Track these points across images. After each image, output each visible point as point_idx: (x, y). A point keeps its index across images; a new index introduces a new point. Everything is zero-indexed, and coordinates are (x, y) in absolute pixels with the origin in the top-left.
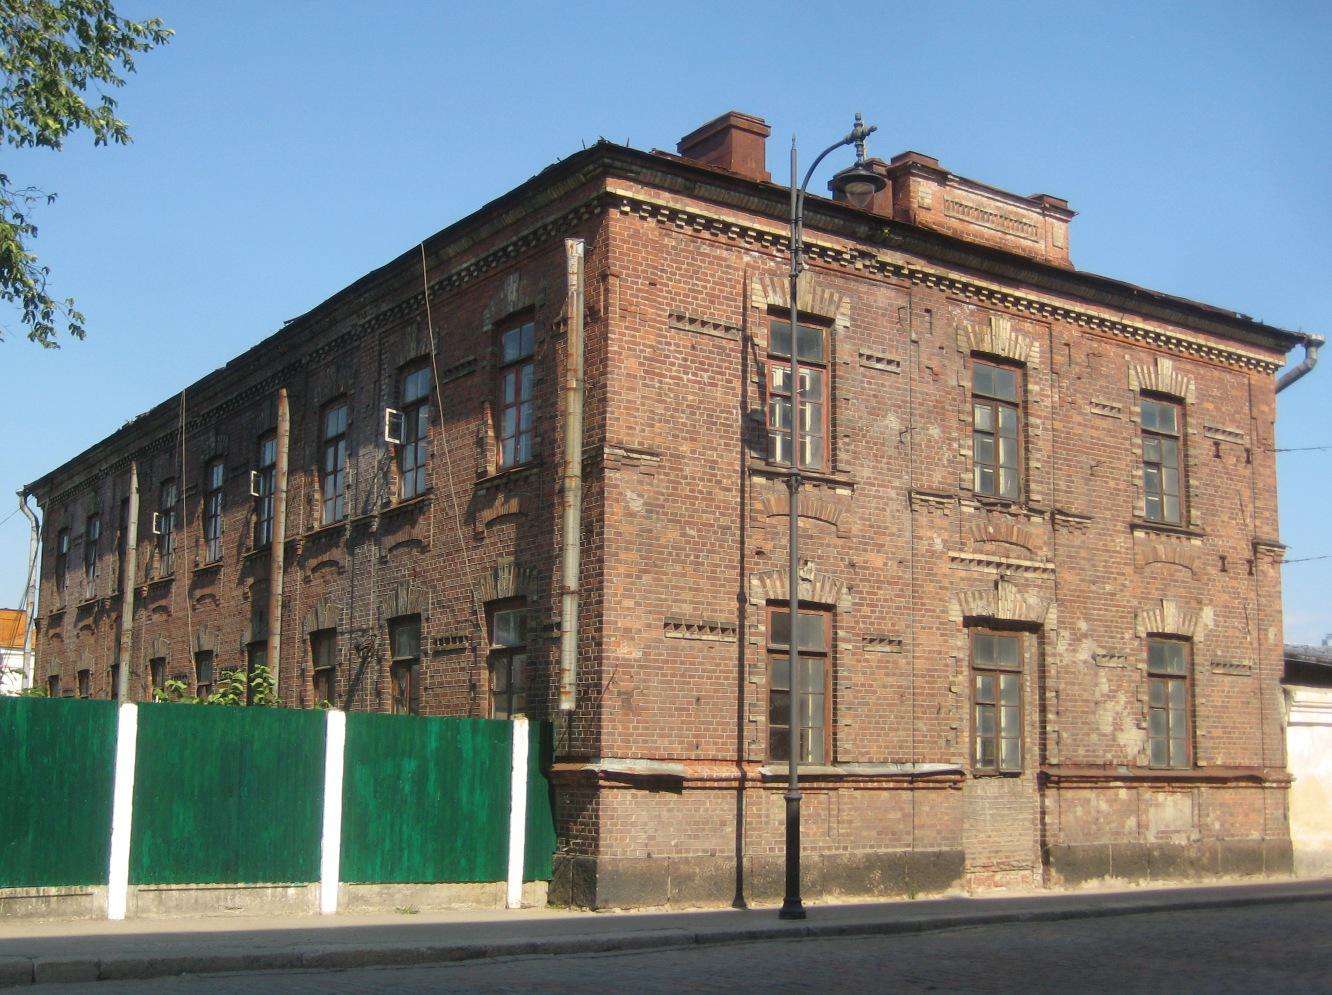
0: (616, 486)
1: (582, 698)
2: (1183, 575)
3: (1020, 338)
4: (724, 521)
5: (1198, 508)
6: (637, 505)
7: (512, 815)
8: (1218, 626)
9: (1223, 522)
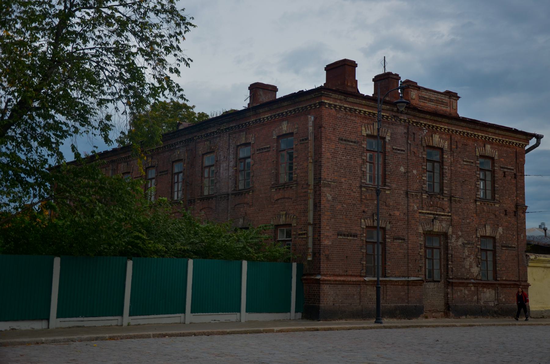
1: (314, 254)
5: (498, 194)
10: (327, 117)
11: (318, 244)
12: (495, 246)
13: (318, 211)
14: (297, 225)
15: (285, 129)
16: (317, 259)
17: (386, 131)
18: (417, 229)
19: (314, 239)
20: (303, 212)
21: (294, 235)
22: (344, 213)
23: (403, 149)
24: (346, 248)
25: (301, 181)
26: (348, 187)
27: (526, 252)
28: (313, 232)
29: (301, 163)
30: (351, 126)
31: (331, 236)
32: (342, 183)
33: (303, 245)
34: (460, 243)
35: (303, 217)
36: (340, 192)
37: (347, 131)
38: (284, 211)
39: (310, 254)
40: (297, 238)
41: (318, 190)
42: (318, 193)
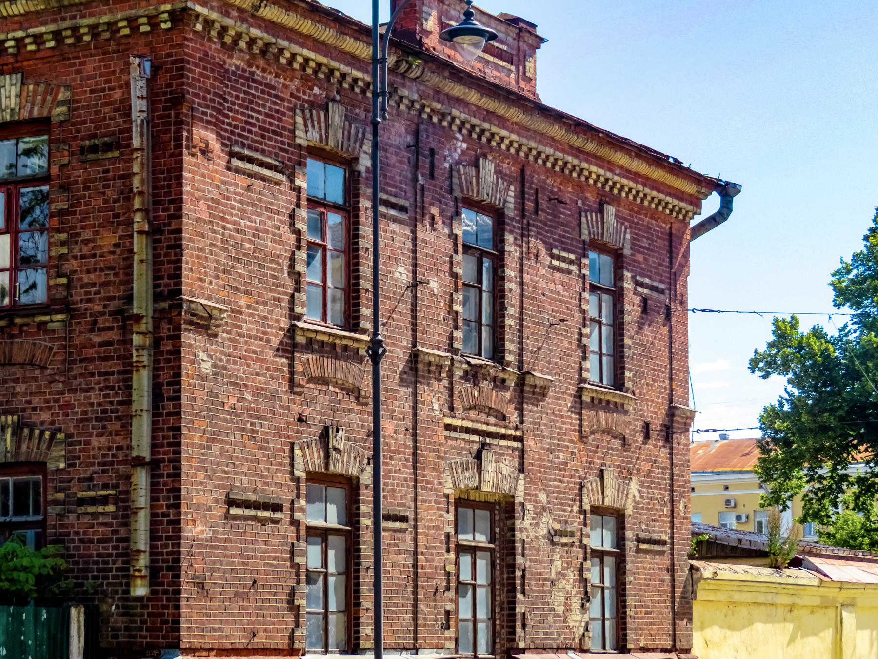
0: (190, 346)
1: (154, 576)
2: (617, 443)
3: (500, 180)
4: (273, 385)
5: (630, 370)
6: (206, 367)
7: (261, 657)
8: (642, 497)
9: (648, 384)
10: (197, 65)
11: (168, 538)
12: (620, 540)
13: (169, 414)
14: (70, 465)
15: (13, 102)
16: (166, 592)
17: (360, 135)
18: (440, 483)
19: (154, 523)
20: (98, 419)
21: (56, 502)
22: (245, 423)
23: (402, 202)
24: (254, 550)
25: (89, 301)
26: (258, 331)
27: (691, 557)
28: (152, 491)
29: (87, 235)
30: (264, 106)
31: (210, 509)
32: (240, 313)
33: (100, 541)
34: (543, 531)
35: (100, 435)
36: (235, 348)
37: (253, 125)
38: (12, 412)
39: (143, 573)
40: (72, 517)
41: (169, 338)
42: (167, 346)
